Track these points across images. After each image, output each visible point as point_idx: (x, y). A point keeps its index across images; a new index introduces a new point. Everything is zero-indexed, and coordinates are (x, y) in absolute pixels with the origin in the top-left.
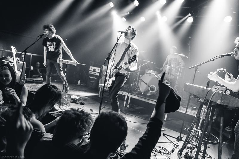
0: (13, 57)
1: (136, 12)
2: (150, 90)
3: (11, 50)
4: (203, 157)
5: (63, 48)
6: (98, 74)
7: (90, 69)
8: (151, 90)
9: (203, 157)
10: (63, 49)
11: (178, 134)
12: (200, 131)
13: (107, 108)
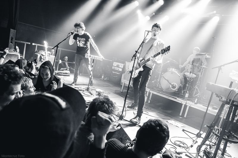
0: (45, 51)
1: (161, 10)
2: (171, 87)
3: (44, 45)
4: (223, 154)
5: (91, 44)
6: (121, 70)
7: (114, 65)
8: (172, 88)
9: (223, 154)
10: (91, 45)
11: (198, 131)
12: (220, 130)
13: (129, 102)
